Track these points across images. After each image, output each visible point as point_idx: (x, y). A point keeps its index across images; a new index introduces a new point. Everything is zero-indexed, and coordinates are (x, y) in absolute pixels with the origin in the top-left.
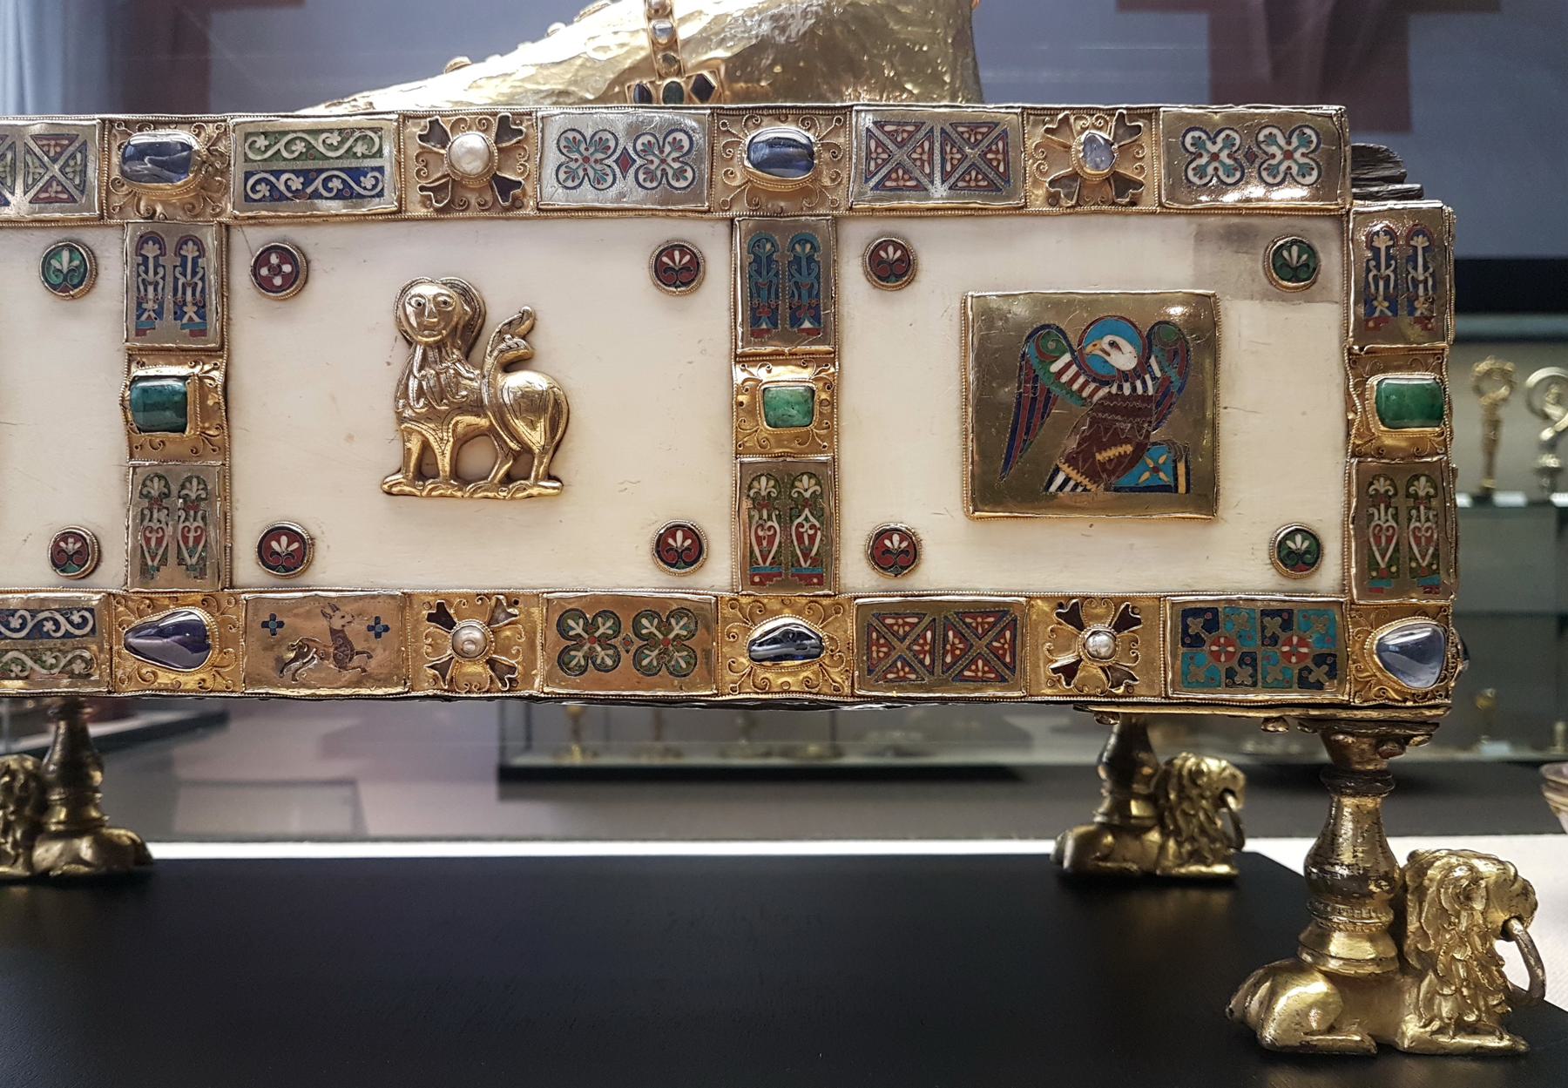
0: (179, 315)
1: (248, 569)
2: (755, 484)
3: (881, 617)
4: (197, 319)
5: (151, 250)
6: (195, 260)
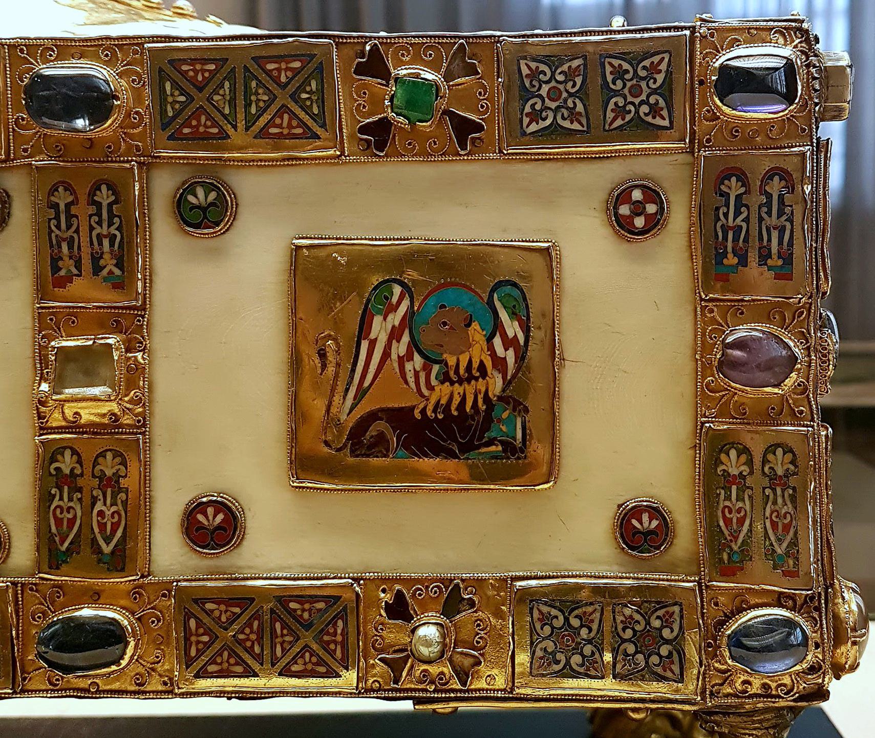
0: (97, 270)
2: (100, 460)
3: (200, 601)
4: (117, 272)
5: (62, 198)
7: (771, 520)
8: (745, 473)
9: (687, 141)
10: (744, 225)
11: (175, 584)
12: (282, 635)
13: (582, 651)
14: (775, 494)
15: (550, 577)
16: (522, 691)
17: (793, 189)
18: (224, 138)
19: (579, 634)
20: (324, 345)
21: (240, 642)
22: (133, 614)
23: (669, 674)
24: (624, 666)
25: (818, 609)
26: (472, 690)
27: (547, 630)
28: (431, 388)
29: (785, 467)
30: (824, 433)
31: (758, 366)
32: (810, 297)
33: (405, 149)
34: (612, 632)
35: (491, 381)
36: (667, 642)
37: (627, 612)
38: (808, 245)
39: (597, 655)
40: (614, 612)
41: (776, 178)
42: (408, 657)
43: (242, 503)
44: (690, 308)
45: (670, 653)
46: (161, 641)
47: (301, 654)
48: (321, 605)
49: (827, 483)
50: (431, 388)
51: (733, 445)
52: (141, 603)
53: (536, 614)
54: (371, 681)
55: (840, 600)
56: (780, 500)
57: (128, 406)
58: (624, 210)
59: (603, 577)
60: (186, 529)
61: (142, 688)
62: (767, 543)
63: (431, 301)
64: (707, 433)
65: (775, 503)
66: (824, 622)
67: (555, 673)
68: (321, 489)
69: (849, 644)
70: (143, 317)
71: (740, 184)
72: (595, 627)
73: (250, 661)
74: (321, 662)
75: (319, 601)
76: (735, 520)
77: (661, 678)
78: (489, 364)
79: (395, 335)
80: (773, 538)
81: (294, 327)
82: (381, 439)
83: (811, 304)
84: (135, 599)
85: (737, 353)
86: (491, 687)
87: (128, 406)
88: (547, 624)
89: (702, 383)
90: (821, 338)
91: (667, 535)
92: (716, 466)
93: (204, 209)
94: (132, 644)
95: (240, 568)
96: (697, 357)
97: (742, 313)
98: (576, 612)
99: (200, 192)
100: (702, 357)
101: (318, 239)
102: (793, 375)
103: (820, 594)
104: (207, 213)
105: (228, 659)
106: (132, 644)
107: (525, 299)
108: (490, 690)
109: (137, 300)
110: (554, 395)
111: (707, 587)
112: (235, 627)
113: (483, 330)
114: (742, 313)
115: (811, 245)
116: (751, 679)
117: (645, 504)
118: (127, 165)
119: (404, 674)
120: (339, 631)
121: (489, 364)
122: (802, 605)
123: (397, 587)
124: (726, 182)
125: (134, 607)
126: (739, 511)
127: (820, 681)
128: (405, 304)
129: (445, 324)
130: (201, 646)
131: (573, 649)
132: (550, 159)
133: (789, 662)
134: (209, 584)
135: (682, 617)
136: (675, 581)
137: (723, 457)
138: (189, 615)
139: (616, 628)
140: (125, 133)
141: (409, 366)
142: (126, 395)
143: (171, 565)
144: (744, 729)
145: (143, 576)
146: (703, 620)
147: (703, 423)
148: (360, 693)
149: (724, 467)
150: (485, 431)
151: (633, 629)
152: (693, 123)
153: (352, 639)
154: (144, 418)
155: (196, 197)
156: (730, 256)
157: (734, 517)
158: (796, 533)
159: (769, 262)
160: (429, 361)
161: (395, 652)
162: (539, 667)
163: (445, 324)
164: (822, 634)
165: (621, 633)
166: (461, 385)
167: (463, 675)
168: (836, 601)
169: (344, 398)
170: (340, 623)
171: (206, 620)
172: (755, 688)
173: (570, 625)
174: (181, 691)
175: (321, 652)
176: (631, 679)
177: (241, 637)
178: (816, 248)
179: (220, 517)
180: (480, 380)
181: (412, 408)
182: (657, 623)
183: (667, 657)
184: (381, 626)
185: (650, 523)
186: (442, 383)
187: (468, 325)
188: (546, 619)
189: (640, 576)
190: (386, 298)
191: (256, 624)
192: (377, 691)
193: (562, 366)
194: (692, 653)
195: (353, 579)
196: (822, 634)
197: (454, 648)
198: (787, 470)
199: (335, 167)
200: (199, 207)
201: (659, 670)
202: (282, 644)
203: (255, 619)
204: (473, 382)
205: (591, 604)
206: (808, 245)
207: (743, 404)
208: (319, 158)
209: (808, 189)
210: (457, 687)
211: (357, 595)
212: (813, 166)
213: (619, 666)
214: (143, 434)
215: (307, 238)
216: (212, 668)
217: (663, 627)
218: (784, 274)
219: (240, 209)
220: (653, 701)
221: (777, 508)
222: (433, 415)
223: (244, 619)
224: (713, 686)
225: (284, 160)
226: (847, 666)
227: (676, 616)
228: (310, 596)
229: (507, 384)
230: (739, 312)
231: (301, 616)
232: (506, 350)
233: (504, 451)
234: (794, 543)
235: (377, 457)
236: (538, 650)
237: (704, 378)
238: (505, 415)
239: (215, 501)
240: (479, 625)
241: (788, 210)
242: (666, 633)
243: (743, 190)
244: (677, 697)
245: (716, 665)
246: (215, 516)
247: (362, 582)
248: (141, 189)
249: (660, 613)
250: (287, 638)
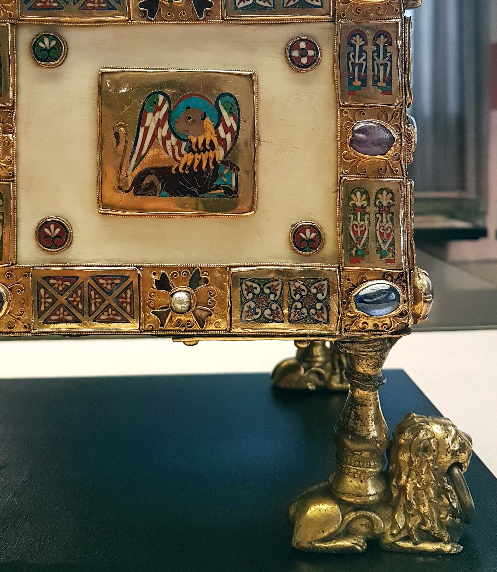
3: (46, 279)
7: (380, 232)
8: (365, 205)
9: (331, 14)
10: (364, 63)
11: (32, 268)
12: (95, 299)
13: (271, 307)
14: (382, 217)
15: (252, 266)
16: (236, 330)
17: (392, 42)
18: (61, 9)
19: (269, 298)
20: (118, 130)
21: (70, 302)
22: (7, 286)
23: (321, 319)
24: (296, 315)
25: (405, 281)
26: (207, 331)
27: (251, 295)
28: (182, 156)
29: (388, 201)
30: (409, 183)
31: (373, 143)
32: (401, 105)
33: (166, 16)
34: (288, 296)
35: (217, 152)
36: (320, 301)
37: (297, 284)
38: (400, 74)
39: (280, 310)
40: (289, 285)
41: (382, 37)
42: (169, 311)
43: (70, 222)
44: (334, 111)
45: (322, 307)
46: (23, 302)
47: (106, 309)
48: (118, 281)
49: (411, 212)
50: (182, 156)
51: (358, 189)
52: (11, 280)
53: (244, 287)
54: (147, 326)
55: (418, 278)
56: (385, 220)
57: (4, 165)
58: (295, 53)
59: (283, 266)
60: (38, 237)
61: (12, 330)
62: (377, 244)
63: (182, 104)
64: (344, 182)
65: (382, 222)
66: (409, 288)
67: (255, 320)
68: (117, 215)
69: (422, 302)
70: (13, 113)
71: (362, 39)
72: (278, 293)
73: (76, 313)
74: (118, 314)
75: (116, 279)
76: (359, 232)
77: (317, 322)
78: (216, 142)
79: (160, 124)
80: (380, 241)
81: (100, 120)
82: (152, 185)
83: (402, 109)
84: (8, 277)
85: (361, 136)
86: (217, 329)
87: (4, 165)
88: (250, 292)
89: (341, 154)
90: (407, 129)
91: (320, 242)
92: (349, 201)
93: (48, 51)
94: (6, 303)
95: (71, 260)
96: (338, 139)
97: (363, 114)
98: (267, 285)
99: (46, 41)
100: (341, 139)
101: (115, 68)
102: (392, 148)
103: (406, 272)
104: (50, 54)
105: (63, 312)
106: (6, 303)
107: (237, 104)
108: (217, 330)
109: (9, 103)
110: (254, 161)
111: (343, 269)
112: (67, 293)
113: (212, 122)
114: (363, 114)
115: (402, 75)
116: (367, 321)
117: (308, 224)
118: (5, 25)
119: (167, 321)
120: (128, 296)
121: (216, 142)
122: (396, 280)
123: (162, 271)
124: (354, 38)
125: (8, 283)
126: (362, 226)
127: (406, 321)
128: (166, 106)
129: (190, 118)
130: (47, 305)
131: (266, 306)
132: (251, 24)
133: (389, 309)
134: (52, 268)
135: (328, 287)
136: (325, 267)
137: (353, 196)
138: (40, 286)
139: (291, 294)
140: (3, 6)
141: (168, 143)
142: (3, 159)
143: (29, 258)
144: (363, 352)
145: (13, 264)
146: (341, 288)
147: (341, 177)
148: (141, 332)
149: (353, 202)
150: (210, 182)
151: (301, 294)
152: (334, 5)
153: (136, 300)
154: (13, 173)
155: (44, 44)
156: (357, 80)
157: (359, 230)
158: (393, 238)
159: (379, 84)
160: (180, 140)
161: (161, 308)
162: (246, 317)
163: (190, 118)
164: (407, 295)
165: (294, 297)
166: (199, 154)
167: (202, 322)
168: (415, 279)
169: (130, 161)
170: (129, 291)
171: (50, 289)
172: (370, 326)
173: (264, 293)
174: (35, 331)
175: (118, 309)
176: (299, 323)
177: (71, 299)
178: (404, 77)
179: (58, 230)
180: (211, 151)
181: (171, 167)
182: (314, 291)
183: (320, 310)
184: (153, 294)
185: (311, 235)
186: (188, 153)
187: (204, 119)
188: (250, 290)
189: (304, 265)
190: (155, 103)
191: (79, 292)
192: (151, 331)
193: (259, 145)
194: (334, 307)
195: (136, 267)
196: (407, 295)
197: (196, 306)
198: (389, 203)
199: (125, 28)
200: (45, 49)
201: (315, 317)
202: (95, 303)
203: (79, 289)
204: (207, 152)
205: (276, 280)
206: (400, 74)
207: (364, 166)
208: (116, 21)
209: (400, 43)
210: (198, 329)
211: (139, 275)
212: (402, 31)
213: (292, 315)
214: (13, 181)
215: (108, 68)
216: (54, 318)
217: (317, 293)
218: (387, 91)
219: (69, 51)
220: (311, 336)
221: (383, 225)
222: (183, 171)
223: (73, 289)
224: (346, 326)
225: (95, 22)
226: (421, 315)
227: (326, 287)
228: (111, 276)
229: (227, 154)
230: (361, 112)
231: (106, 287)
232: (226, 134)
233: (225, 193)
234: (392, 244)
235: (150, 196)
236: (245, 306)
237: (342, 151)
238: (226, 172)
239: (55, 221)
240: (210, 293)
241: (389, 55)
242: (319, 296)
243: (363, 43)
244: (326, 332)
245: (348, 314)
246: (55, 230)
247: (141, 268)
248: (12, 38)
249: (316, 285)
250: (98, 300)
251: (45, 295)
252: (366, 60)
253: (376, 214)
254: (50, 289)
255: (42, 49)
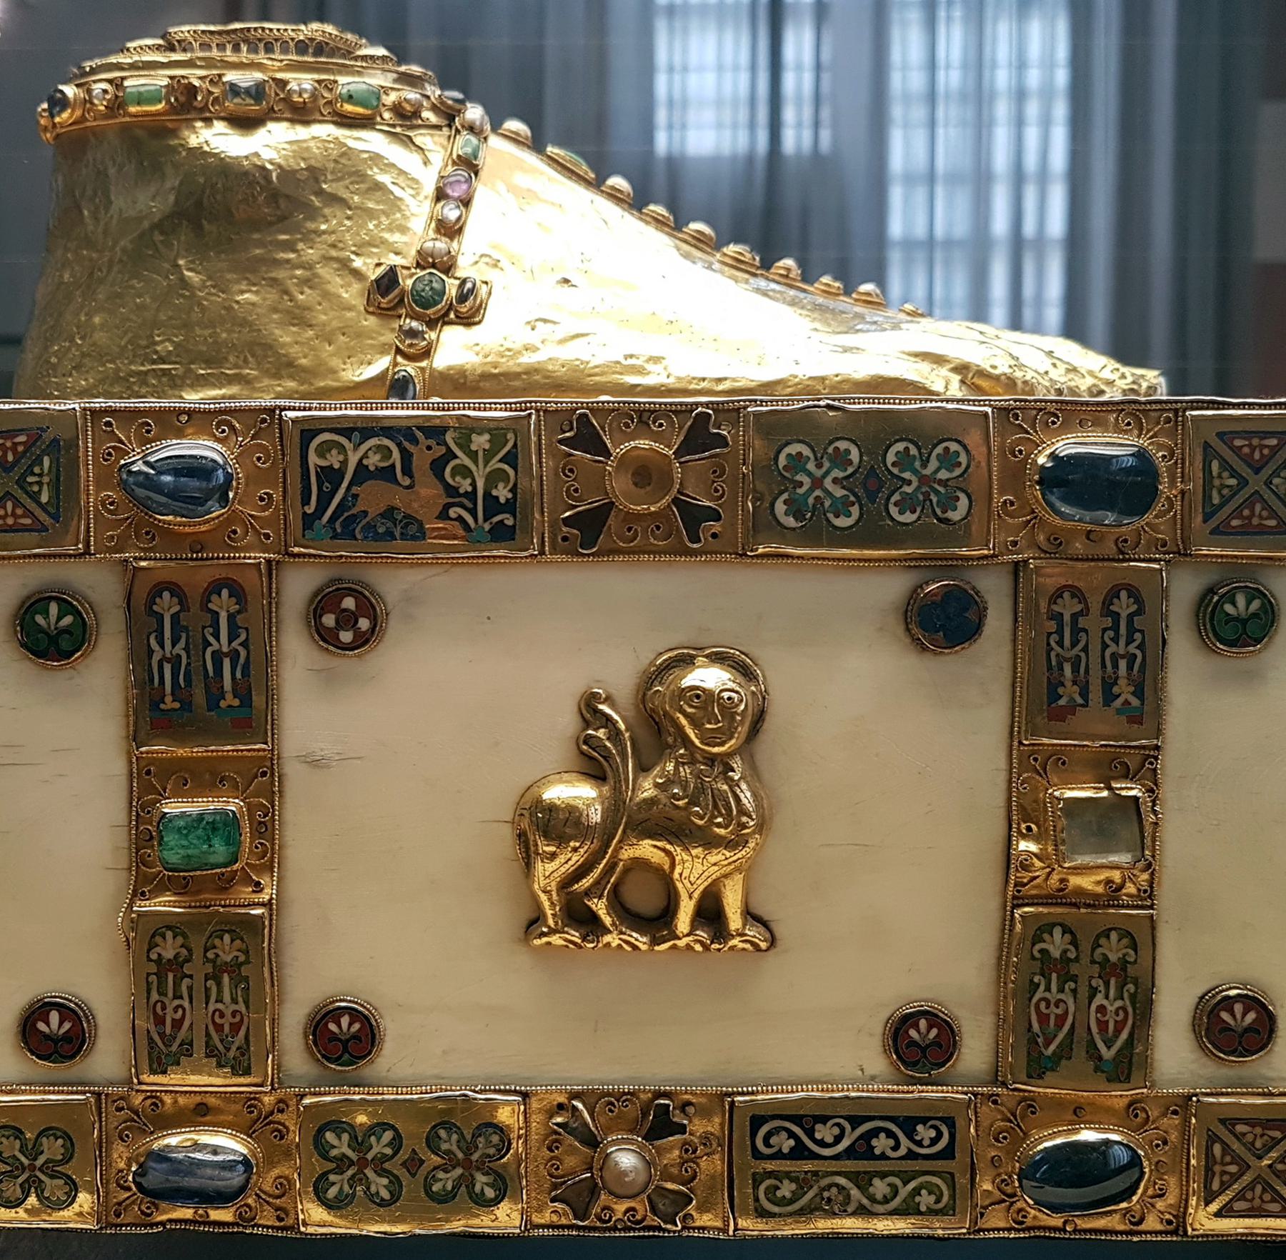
0: (1109, 698)
1: (295, 1055)
4: (1135, 702)
6: (175, 618)
10: (1138, 653)
26: (984, 1230)
95: (1273, 1080)
130: (1226, 1178)
171: (1236, 1146)
179: (1251, 1016)
200: (1236, 619)
246: (1244, 1015)
251: (1223, 1156)
252: (1085, 649)
253: (148, 974)
254: (1236, 1146)
255: (1230, 619)
